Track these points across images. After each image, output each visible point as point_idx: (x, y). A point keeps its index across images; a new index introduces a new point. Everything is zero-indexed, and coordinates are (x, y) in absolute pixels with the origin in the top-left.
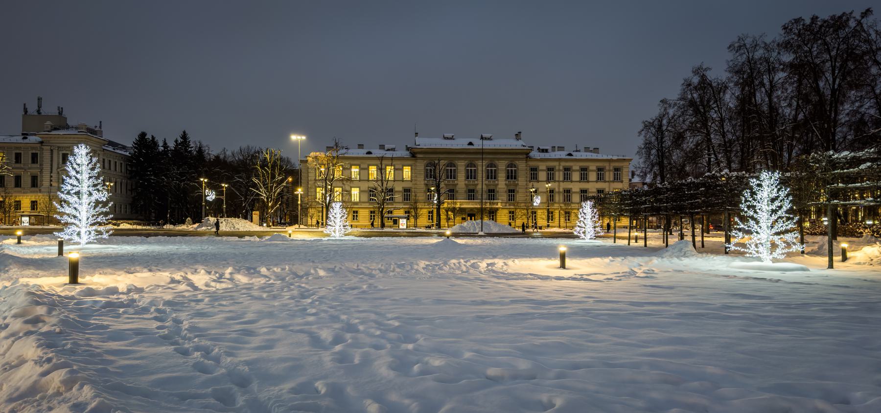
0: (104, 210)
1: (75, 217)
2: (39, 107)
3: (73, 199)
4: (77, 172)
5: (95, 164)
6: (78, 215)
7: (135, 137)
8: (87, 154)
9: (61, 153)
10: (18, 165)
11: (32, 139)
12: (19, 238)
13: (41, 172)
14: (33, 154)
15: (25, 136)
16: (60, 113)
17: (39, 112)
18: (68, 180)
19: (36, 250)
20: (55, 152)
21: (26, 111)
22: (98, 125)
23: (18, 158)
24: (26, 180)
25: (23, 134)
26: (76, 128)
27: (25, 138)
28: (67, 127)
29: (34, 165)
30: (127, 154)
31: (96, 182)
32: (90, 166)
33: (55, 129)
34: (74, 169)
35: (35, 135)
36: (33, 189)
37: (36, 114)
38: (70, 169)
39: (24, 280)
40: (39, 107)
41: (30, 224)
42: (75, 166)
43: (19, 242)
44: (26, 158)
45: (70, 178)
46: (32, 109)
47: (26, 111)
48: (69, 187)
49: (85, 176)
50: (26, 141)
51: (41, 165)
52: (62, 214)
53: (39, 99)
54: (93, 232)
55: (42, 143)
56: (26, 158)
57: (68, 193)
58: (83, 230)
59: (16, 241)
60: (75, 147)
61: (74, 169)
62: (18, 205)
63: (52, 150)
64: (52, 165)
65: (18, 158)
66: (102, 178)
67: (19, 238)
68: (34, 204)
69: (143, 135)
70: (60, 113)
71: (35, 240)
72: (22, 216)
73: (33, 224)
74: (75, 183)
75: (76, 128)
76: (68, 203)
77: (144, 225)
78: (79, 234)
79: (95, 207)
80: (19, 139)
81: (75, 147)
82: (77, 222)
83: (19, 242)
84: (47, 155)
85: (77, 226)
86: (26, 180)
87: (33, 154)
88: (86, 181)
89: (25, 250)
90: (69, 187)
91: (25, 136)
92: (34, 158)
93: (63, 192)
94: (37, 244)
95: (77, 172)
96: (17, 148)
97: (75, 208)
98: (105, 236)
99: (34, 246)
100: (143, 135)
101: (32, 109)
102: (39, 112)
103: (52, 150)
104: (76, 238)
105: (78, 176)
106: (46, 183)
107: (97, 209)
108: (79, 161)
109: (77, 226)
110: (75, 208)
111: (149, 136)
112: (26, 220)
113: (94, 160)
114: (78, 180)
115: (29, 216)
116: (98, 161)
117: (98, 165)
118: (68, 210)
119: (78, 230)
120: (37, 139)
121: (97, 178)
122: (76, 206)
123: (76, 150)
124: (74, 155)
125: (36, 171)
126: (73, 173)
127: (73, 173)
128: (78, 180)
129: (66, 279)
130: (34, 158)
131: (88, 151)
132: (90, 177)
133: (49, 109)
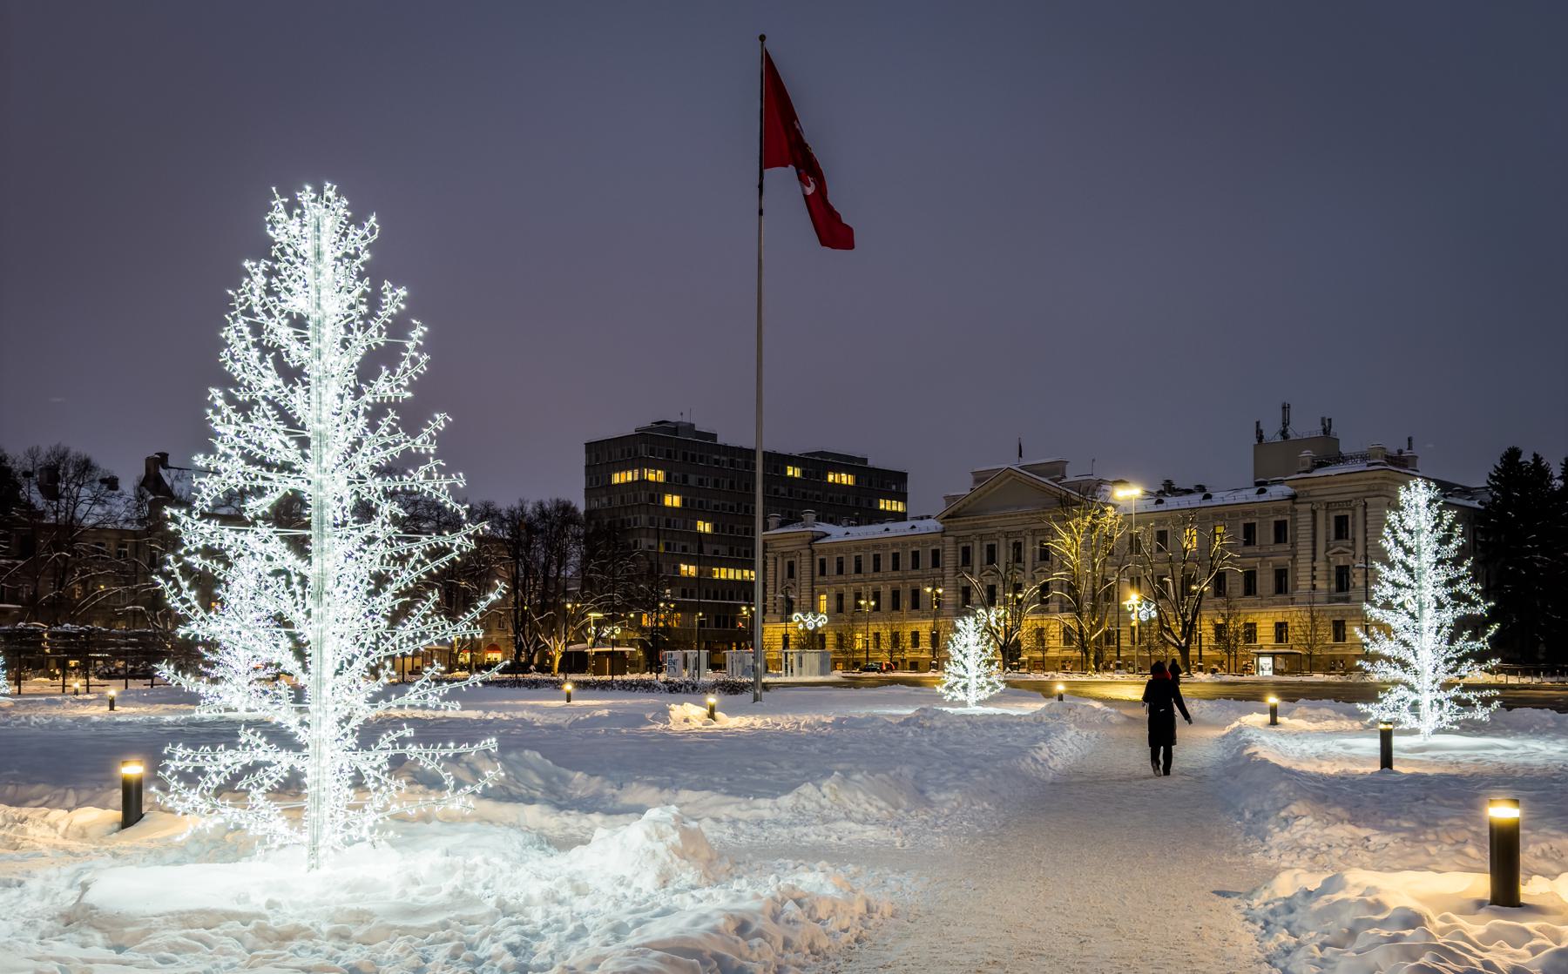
0: (1478, 645)
1: (1404, 665)
2: (1286, 424)
3: (1397, 621)
4: (1408, 551)
5: (1451, 528)
6: (1412, 660)
7: (1493, 462)
8: (1431, 501)
9: (1332, 516)
10: (1249, 549)
11: (1276, 492)
12: (1274, 711)
13: (1294, 560)
14: (1246, 525)
15: (1261, 487)
16: (1326, 431)
17: (1284, 434)
18: (1385, 571)
19: (1318, 745)
20: (1321, 515)
21: (1260, 438)
22: (1405, 447)
23: (1249, 531)
24: (1266, 581)
25: (1257, 484)
26: (1364, 457)
27: (1262, 491)
28: (1340, 459)
29: (1280, 547)
30: (1476, 504)
31: (1453, 574)
32: (1439, 534)
33: (1321, 465)
34: (1399, 543)
35: (1281, 482)
36: (1279, 597)
37: (1279, 439)
38: (1388, 545)
39: (1360, 880)
40: (1286, 424)
41: (1276, 671)
42: (1402, 536)
43: (1274, 723)
44: (1266, 534)
45: (1391, 566)
46: (1272, 433)
47: (1260, 438)
48: (1389, 590)
49: (1428, 558)
50: (1264, 497)
51: (1293, 545)
52: (1373, 658)
53: (1286, 408)
54: (1447, 704)
55: (1293, 497)
56: (1266, 534)
57: (1387, 605)
58: (1426, 699)
59: (1267, 717)
60: (1402, 490)
61: (1399, 543)
62: (1251, 632)
63: (1314, 512)
64: (1314, 543)
65: (1249, 531)
66: (1468, 563)
67: (1274, 711)
68: (1281, 630)
69: (1512, 455)
70: (1326, 431)
71: (1304, 717)
72: (1259, 655)
73: (1282, 673)
74: (277, 444)
75: (1364, 457)
76: (1387, 630)
77: (1526, 673)
78: (1415, 706)
79: (1451, 642)
80: (1251, 494)
81: (1402, 490)
82: (1411, 679)
83: (1274, 723)
84: (1304, 519)
85: (1412, 689)
86: (1266, 581)
87: (1246, 525)
88: (1430, 572)
89: (1294, 746)
90: (1389, 590)
91: (1261, 487)
92: (1281, 531)
93: (1374, 604)
94: (1313, 726)
95: (1408, 551)
96: (1246, 514)
97: (1405, 643)
98: (1481, 714)
99: (1307, 734)
100: (1512, 455)
101: (1272, 433)
102: (1284, 434)
103: (1314, 512)
104: (1409, 721)
105: (1411, 561)
106: (1304, 583)
107: (1458, 644)
108: (1410, 523)
109: (1412, 689)
110: (1405, 643)
111: (1526, 458)
112: (1266, 662)
113: (1449, 516)
114: (1409, 570)
115: (1273, 655)
116: (1456, 520)
117: (1459, 529)
118: (1387, 648)
119: (1412, 697)
120: (1286, 490)
121: (1457, 562)
122: (1406, 636)
123: (1403, 495)
124: (1397, 508)
125: (1283, 560)
126: (1399, 554)
127: (1397, 554)
128: (1409, 570)
129: (1481, 884)
130: (1281, 531)
131: (1432, 494)
132: (1441, 562)
133: (1305, 426)
